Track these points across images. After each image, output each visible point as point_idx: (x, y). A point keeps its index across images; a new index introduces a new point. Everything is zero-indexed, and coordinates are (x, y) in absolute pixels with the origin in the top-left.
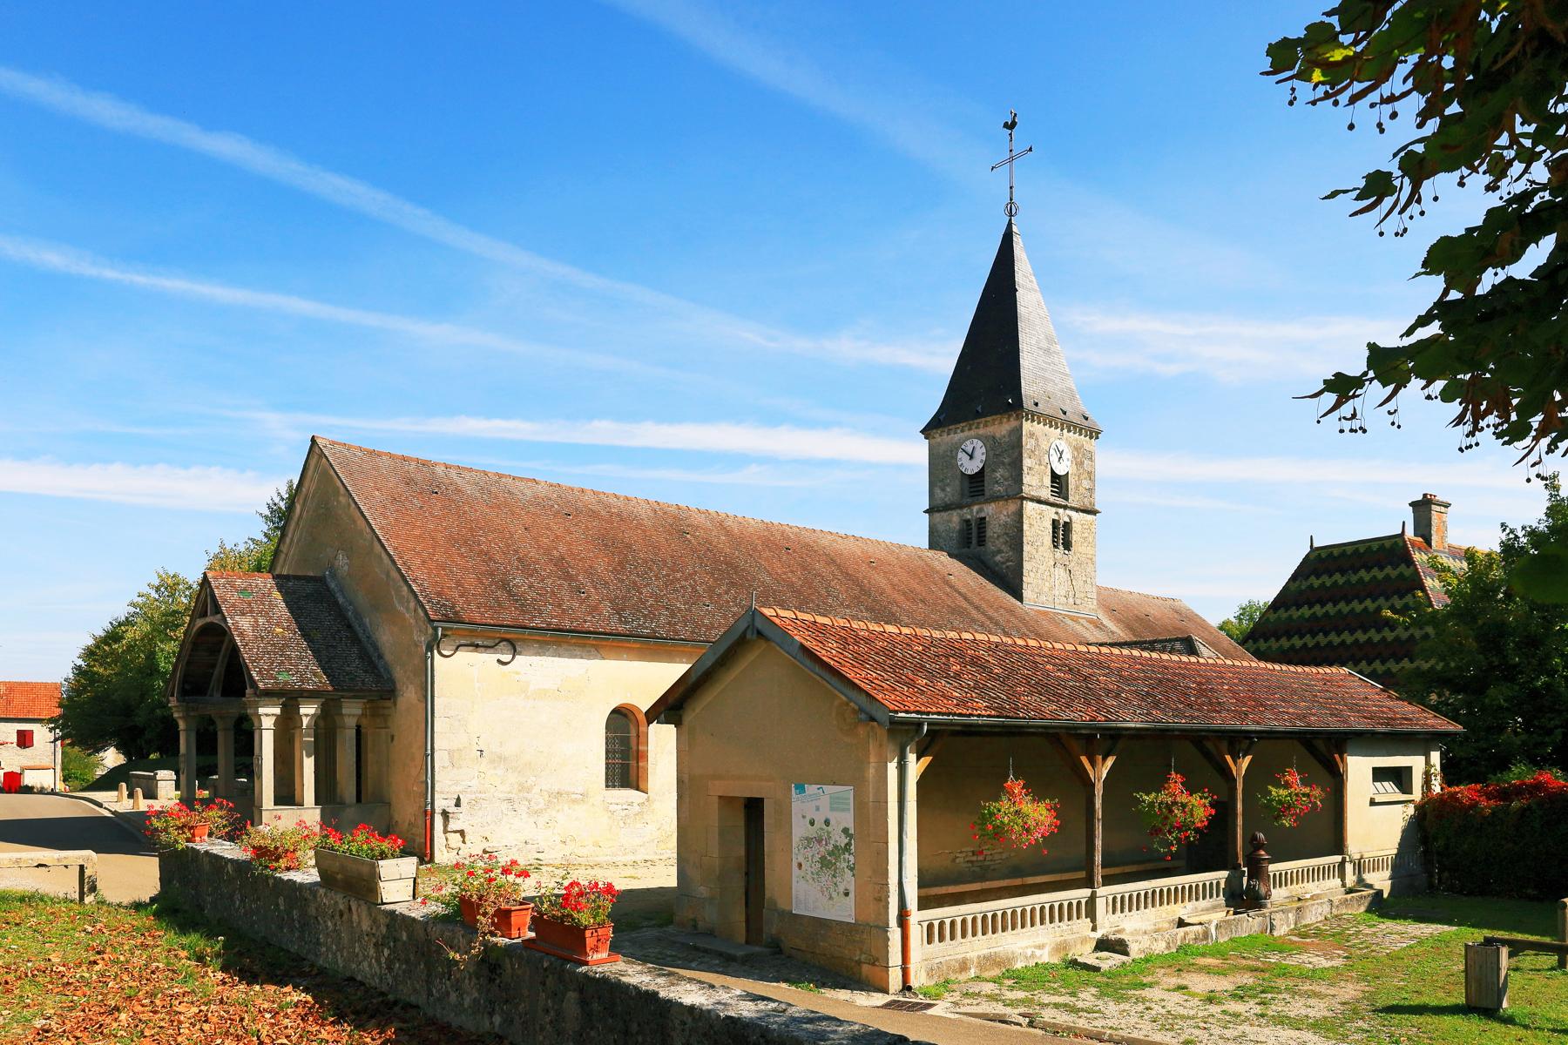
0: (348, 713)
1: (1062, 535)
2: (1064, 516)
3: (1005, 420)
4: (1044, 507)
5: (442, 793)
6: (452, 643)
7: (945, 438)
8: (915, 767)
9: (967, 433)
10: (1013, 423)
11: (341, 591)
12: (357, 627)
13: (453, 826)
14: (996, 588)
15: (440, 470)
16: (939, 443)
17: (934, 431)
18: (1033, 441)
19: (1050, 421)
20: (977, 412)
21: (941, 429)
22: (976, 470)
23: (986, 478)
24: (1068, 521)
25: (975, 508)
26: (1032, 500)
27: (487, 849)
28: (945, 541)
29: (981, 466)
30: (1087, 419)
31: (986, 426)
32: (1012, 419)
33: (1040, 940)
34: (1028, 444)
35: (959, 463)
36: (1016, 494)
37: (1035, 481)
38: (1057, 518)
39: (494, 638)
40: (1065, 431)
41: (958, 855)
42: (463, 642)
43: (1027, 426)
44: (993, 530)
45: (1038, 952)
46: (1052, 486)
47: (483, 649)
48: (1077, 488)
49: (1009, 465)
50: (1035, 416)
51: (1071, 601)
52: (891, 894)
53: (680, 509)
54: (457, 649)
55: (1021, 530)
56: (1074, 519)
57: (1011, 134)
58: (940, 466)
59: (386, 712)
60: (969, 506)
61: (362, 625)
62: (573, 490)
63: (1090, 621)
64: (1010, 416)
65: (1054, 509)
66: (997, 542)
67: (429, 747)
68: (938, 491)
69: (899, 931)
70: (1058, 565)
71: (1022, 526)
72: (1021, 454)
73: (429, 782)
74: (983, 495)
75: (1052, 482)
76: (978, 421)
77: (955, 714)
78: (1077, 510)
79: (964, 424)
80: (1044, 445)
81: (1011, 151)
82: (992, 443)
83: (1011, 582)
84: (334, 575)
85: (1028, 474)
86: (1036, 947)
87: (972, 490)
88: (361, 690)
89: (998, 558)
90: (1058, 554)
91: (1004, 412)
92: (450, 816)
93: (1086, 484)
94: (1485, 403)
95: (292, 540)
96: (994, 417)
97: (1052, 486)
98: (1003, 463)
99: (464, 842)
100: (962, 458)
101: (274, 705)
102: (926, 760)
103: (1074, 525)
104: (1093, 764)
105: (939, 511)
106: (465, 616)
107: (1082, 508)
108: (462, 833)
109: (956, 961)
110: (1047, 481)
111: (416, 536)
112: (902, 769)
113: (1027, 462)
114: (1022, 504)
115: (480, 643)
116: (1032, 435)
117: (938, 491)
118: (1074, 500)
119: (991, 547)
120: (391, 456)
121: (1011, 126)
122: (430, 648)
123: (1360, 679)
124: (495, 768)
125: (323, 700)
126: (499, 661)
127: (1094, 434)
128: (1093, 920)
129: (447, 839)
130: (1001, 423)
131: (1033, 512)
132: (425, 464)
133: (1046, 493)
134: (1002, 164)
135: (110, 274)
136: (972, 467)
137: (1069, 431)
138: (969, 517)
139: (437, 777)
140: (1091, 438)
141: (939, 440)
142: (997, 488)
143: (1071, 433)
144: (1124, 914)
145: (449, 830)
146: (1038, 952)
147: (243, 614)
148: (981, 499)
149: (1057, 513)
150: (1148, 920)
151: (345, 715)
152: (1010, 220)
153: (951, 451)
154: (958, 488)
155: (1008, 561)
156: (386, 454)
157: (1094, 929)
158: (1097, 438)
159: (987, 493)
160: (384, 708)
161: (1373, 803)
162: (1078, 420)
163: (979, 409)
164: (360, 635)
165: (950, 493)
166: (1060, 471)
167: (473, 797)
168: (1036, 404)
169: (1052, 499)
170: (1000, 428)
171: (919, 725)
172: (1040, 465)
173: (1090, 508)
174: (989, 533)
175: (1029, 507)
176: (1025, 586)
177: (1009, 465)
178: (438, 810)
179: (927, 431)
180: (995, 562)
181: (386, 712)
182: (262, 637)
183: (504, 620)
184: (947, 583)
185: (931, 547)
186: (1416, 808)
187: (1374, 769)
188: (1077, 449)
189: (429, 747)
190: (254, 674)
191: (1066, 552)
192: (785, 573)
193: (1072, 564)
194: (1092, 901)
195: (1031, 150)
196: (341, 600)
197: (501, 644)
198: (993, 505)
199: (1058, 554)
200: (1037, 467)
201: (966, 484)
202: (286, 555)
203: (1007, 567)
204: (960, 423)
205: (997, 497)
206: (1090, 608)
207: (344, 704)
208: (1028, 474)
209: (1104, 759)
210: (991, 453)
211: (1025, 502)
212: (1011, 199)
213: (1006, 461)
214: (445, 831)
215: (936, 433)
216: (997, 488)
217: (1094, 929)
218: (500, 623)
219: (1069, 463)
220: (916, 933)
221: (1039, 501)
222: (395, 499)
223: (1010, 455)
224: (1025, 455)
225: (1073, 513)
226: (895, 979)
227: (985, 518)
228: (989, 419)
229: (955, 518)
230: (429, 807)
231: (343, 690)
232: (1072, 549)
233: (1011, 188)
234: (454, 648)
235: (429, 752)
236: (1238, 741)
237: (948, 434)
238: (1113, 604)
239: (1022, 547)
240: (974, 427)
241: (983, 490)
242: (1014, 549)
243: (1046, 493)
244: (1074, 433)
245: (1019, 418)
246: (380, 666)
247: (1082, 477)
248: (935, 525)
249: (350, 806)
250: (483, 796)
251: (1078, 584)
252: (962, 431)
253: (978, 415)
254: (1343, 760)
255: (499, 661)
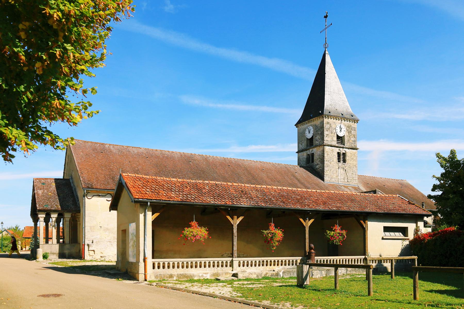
0: (67, 217)
1: (342, 158)
2: (342, 151)
3: (319, 119)
4: (333, 148)
5: (87, 239)
6: (92, 195)
7: (302, 127)
8: (150, 217)
9: (308, 124)
10: (321, 119)
11: (73, 183)
12: (75, 193)
13: (90, 249)
14: (317, 178)
15: (107, 146)
16: (300, 129)
17: (299, 125)
18: (329, 125)
19: (336, 117)
20: (311, 117)
21: (300, 124)
22: (311, 137)
23: (314, 139)
24: (345, 152)
25: (311, 150)
26: (328, 146)
27: (102, 256)
28: (302, 162)
29: (312, 135)
30: (353, 116)
31: (313, 121)
32: (321, 118)
33: (207, 272)
34: (326, 126)
35: (306, 135)
36: (322, 145)
37: (330, 138)
38: (339, 151)
39: (106, 193)
40: (343, 121)
41: (224, 254)
42: (95, 194)
43: (326, 120)
44: (316, 157)
45: (205, 275)
46: (337, 140)
47: (102, 196)
48: (349, 141)
49: (320, 134)
50: (329, 116)
51: (346, 180)
52: (141, 252)
53: (191, 155)
54: (93, 196)
55: (324, 156)
56: (347, 152)
57: (326, 19)
58: (301, 135)
59: (79, 217)
60: (309, 149)
61: (76, 192)
62: (153, 150)
63: (353, 187)
64: (320, 117)
65: (338, 149)
66: (317, 161)
67: (84, 225)
68: (300, 145)
69: (143, 263)
70: (340, 168)
71: (324, 155)
72: (323, 130)
73: (84, 235)
74: (313, 145)
75: (337, 139)
76: (311, 120)
77: (163, 200)
78: (348, 148)
79: (307, 121)
80: (333, 126)
81: (326, 25)
82: (316, 127)
83: (320, 175)
84: (72, 178)
85: (326, 137)
86: (204, 273)
87: (311, 144)
88: (70, 210)
89: (317, 167)
90: (340, 164)
91: (318, 116)
92: (90, 246)
93: (353, 139)
94: (38, 85)
95: (67, 169)
96: (315, 118)
97: (337, 140)
98: (318, 134)
99: (94, 254)
100: (307, 132)
101: (43, 214)
102: (156, 215)
103: (347, 154)
104: (233, 219)
105: (300, 152)
106: (94, 187)
107: (350, 148)
108: (94, 251)
109: (168, 274)
110: (335, 139)
111: (89, 165)
112: (145, 216)
113: (326, 133)
114: (324, 147)
115: (100, 195)
116: (328, 123)
117: (300, 145)
118: (347, 145)
119: (315, 163)
120: (91, 142)
121: (326, 17)
122: (84, 196)
123: (402, 198)
124: (105, 232)
125: (58, 213)
126: (107, 200)
127: (356, 121)
128: (233, 268)
129: (89, 253)
130: (318, 120)
131: (329, 150)
132: (102, 144)
133: (335, 143)
134: (323, 30)
135: (211, 105)
136: (309, 136)
137: (345, 121)
138: (309, 153)
139: (86, 235)
140: (355, 123)
141: (300, 127)
142: (317, 142)
143: (356, 124)
144: (248, 267)
145: (89, 250)
146: (205, 275)
147: (41, 189)
148: (312, 147)
149: (339, 150)
150: (259, 270)
151: (65, 217)
152: (325, 49)
153: (304, 131)
154: (306, 144)
155: (320, 167)
156: (90, 142)
157: (232, 270)
158: (357, 123)
159: (314, 145)
160: (78, 215)
161: (383, 239)
162: (348, 117)
163: (311, 116)
164: (75, 195)
165: (304, 146)
166: (341, 135)
167: (98, 240)
168: (330, 112)
169: (337, 145)
170: (317, 122)
171: (147, 203)
172: (332, 133)
173: (354, 147)
174: (315, 158)
175: (327, 148)
176: (325, 176)
177: (320, 134)
178: (86, 244)
179: (296, 125)
180: (316, 168)
181: (79, 217)
182: (44, 196)
183: (108, 187)
184: (294, 176)
185: (298, 165)
186: (410, 242)
187: (384, 227)
188: (349, 127)
189: (84, 225)
190: (37, 205)
191: (344, 163)
192: (224, 173)
193: (347, 168)
194: (232, 262)
195: (331, 24)
196: (72, 185)
197: (108, 195)
198: (316, 148)
199: (340, 164)
200: (330, 134)
201: (309, 142)
202: (66, 174)
203: (320, 170)
204: (306, 121)
205: (317, 145)
206: (355, 182)
207: (65, 214)
208: (326, 137)
209: (238, 218)
210: (315, 130)
211: (325, 147)
212: (326, 42)
213: (319, 133)
214: (89, 250)
215: (299, 125)
216: (317, 142)
217: (232, 270)
218: (106, 188)
219: (345, 132)
220: (149, 266)
221: (331, 146)
222: (87, 155)
223: (320, 130)
224: (325, 130)
225: (347, 150)
226: (141, 277)
227: (313, 153)
228: (314, 119)
229: (305, 154)
230: (84, 243)
231: (65, 210)
232: (347, 162)
233: (326, 38)
234: (92, 196)
235: (84, 227)
236: (305, 214)
237: (303, 125)
238: (362, 179)
239: (324, 162)
240: (312, 121)
241: (313, 144)
242: (322, 163)
243: (335, 143)
244: (347, 121)
245: (323, 117)
246: (77, 203)
247: (351, 137)
248: (299, 157)
249: (67, 244)
250: (101, 240)
251: (349, 174)
252: (307, 124)
253: (311, 118)
254: (365, 223)
255: (107, 200)
